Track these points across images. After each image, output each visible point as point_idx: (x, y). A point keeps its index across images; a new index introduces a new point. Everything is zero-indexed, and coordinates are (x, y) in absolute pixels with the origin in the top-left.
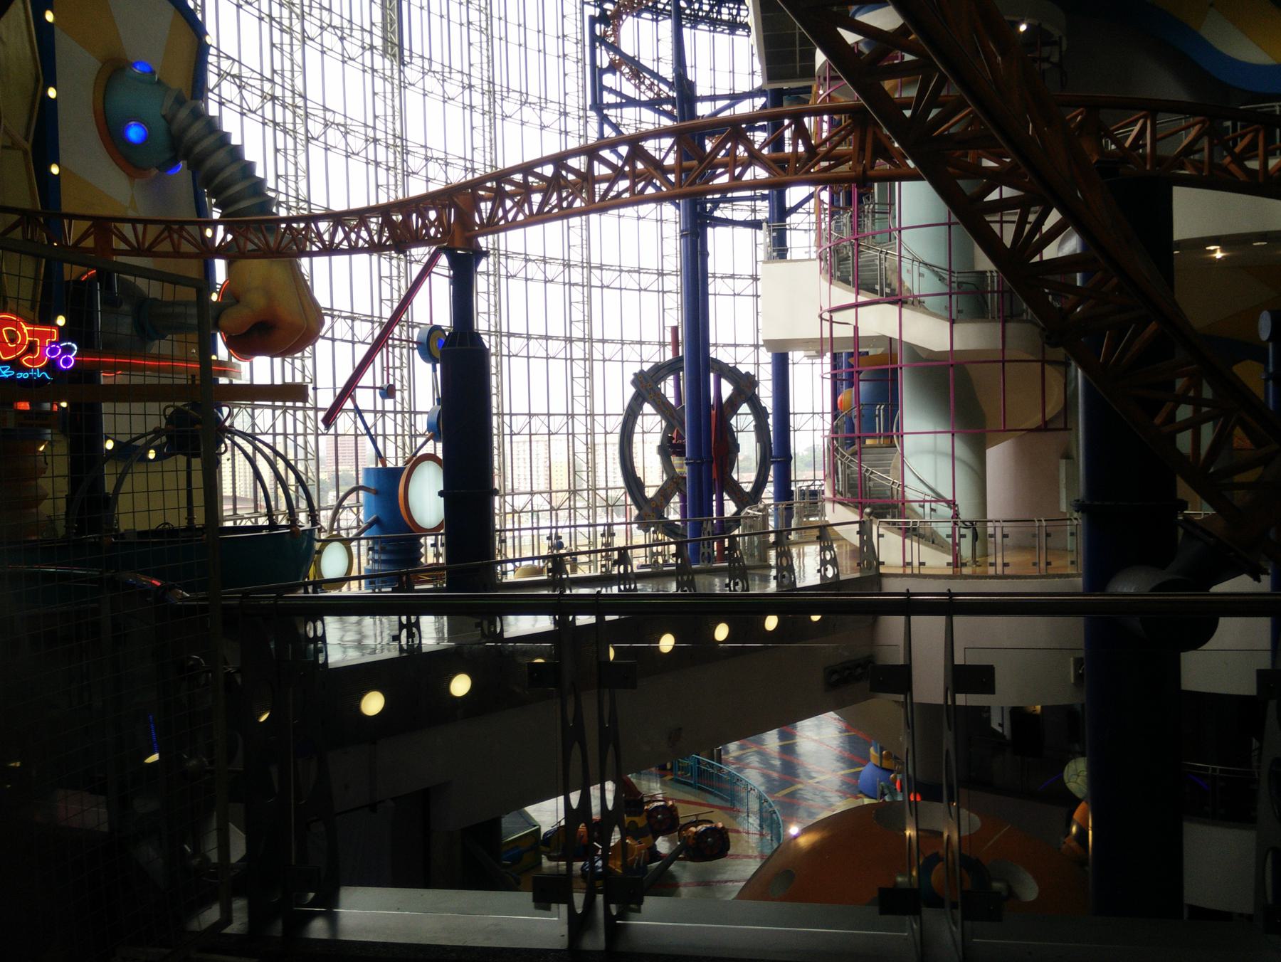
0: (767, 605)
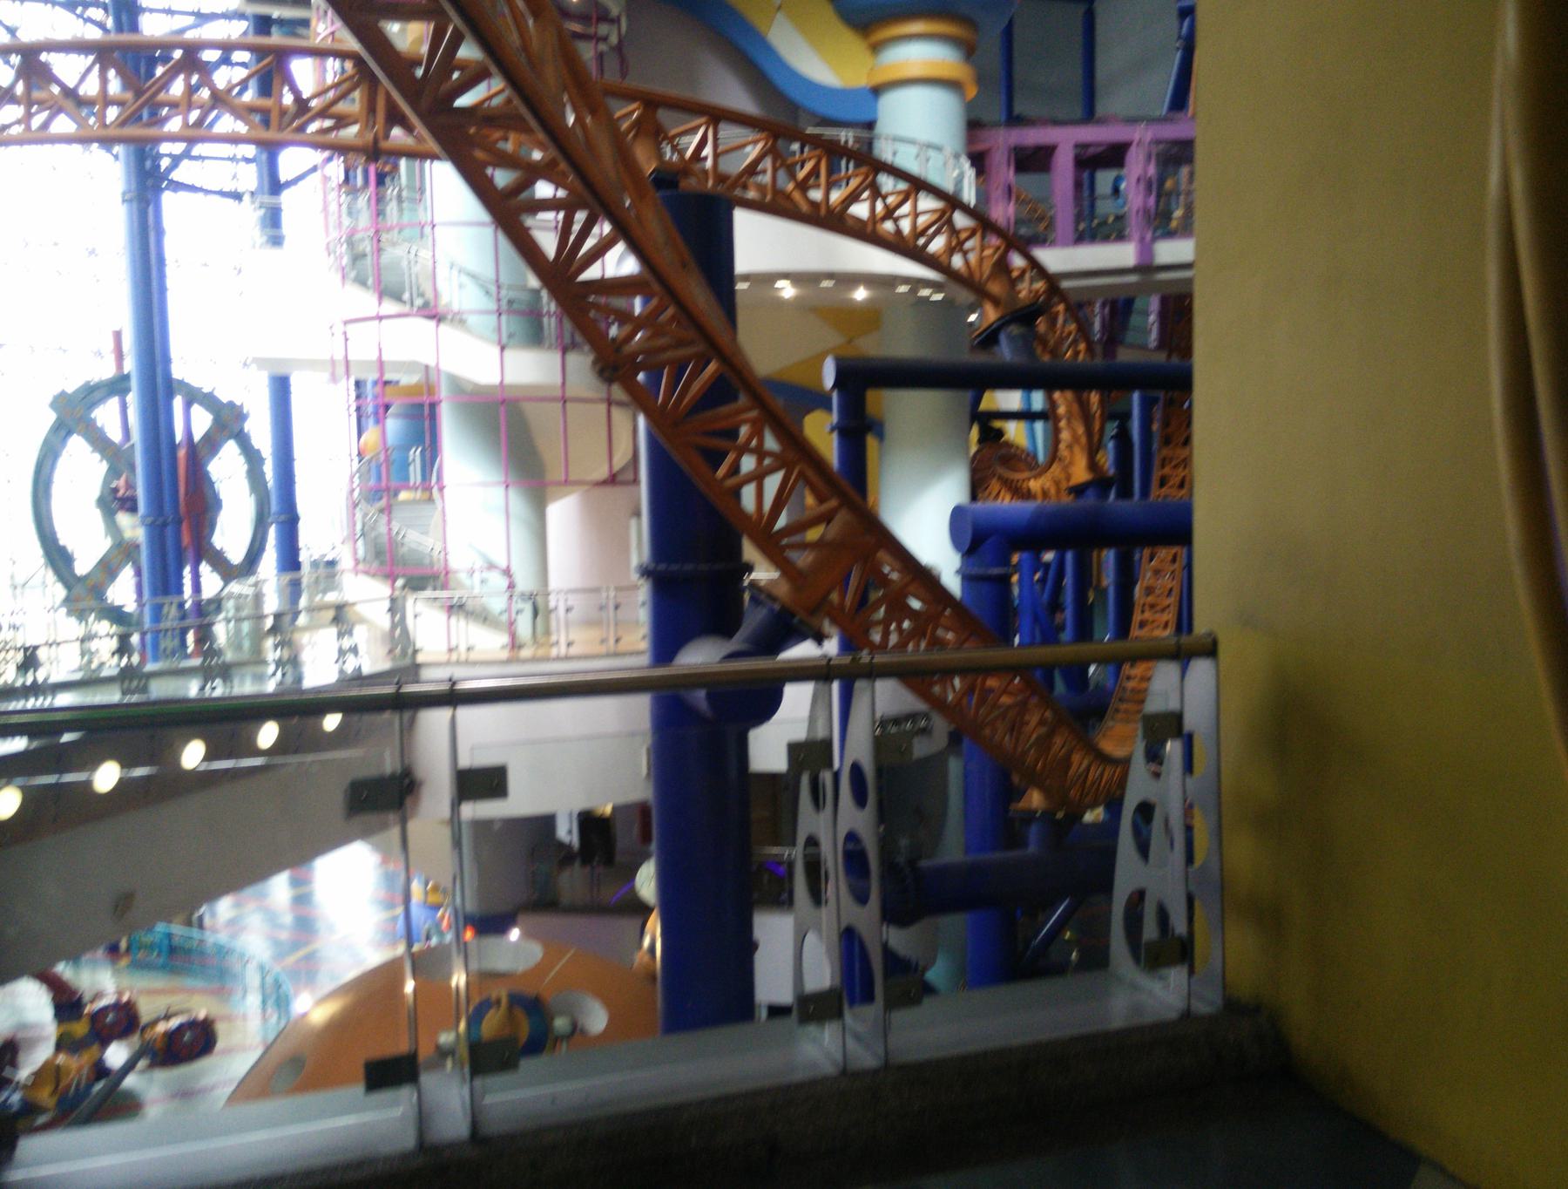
0: (258, 710)
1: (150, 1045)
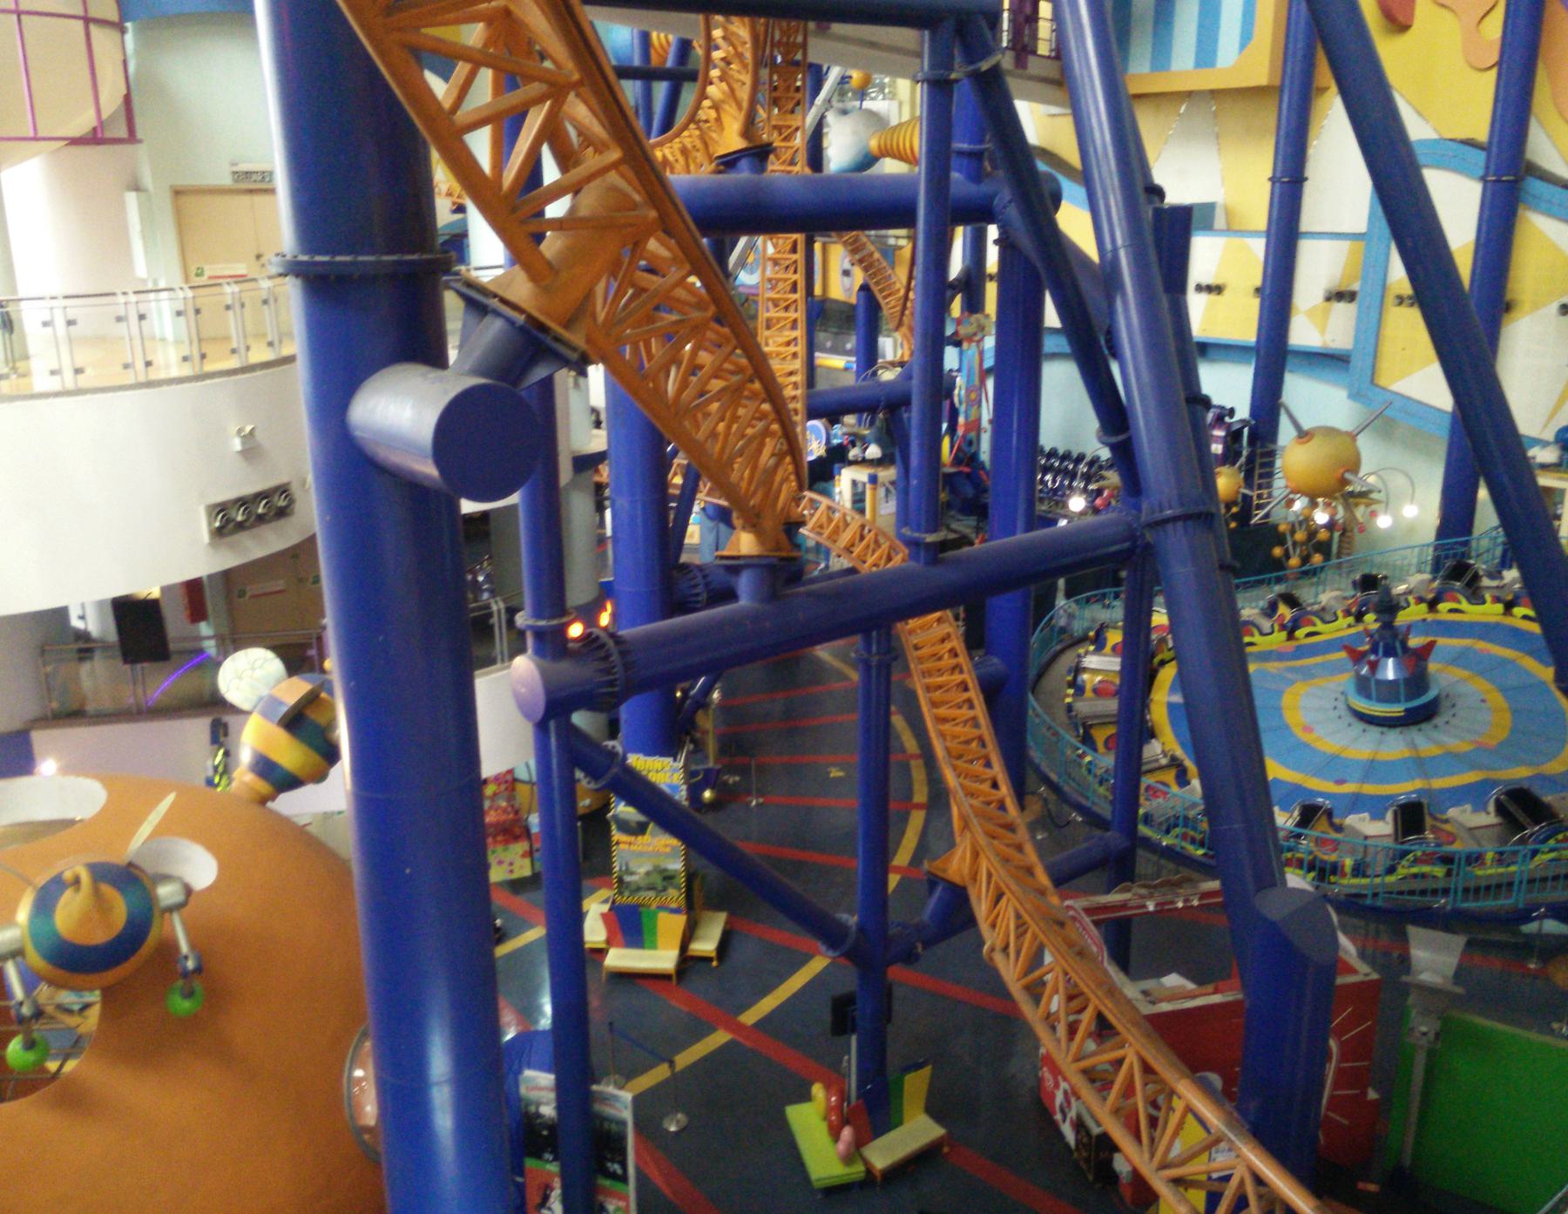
1: (883, 147)
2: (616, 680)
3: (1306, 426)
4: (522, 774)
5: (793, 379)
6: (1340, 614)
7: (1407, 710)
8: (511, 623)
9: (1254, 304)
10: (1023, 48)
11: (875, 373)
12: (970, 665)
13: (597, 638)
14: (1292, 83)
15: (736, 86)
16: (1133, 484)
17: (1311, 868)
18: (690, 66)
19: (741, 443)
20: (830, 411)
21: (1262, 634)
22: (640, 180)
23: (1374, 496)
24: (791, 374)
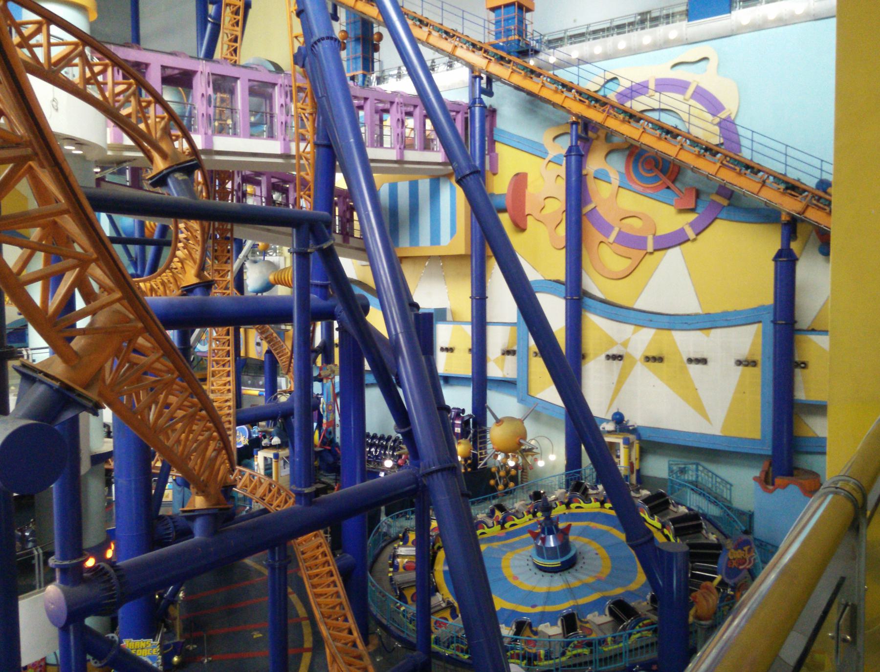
2: (114, 594)
3: (499, 417)
4: (52, 660)
5: (228, 404)
6: (525, 513)
7: (562, 563)
8: (46, 563)
9: (469, 357)
10: (347, 234)
11: (276, 398)
12: (334, 561)
13: (103, 568)
14: (476, 254)
15: (193, 252)
16: (415, 453)
17: (524, 658)
18: (168, 238)
19: (195, 445)
20: (250, 420)
21: (489, 527)
22: (132, 307)
23: (535, 450)
24: (227, 401)
